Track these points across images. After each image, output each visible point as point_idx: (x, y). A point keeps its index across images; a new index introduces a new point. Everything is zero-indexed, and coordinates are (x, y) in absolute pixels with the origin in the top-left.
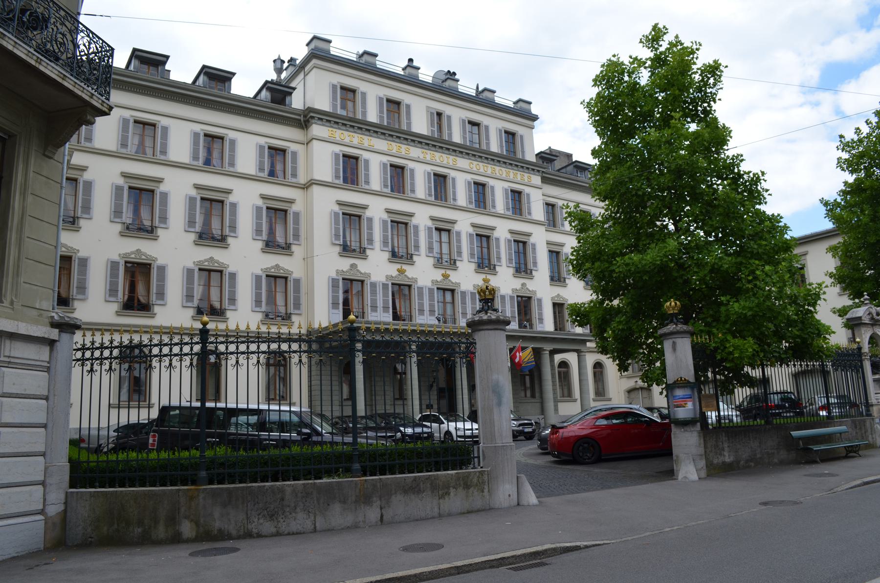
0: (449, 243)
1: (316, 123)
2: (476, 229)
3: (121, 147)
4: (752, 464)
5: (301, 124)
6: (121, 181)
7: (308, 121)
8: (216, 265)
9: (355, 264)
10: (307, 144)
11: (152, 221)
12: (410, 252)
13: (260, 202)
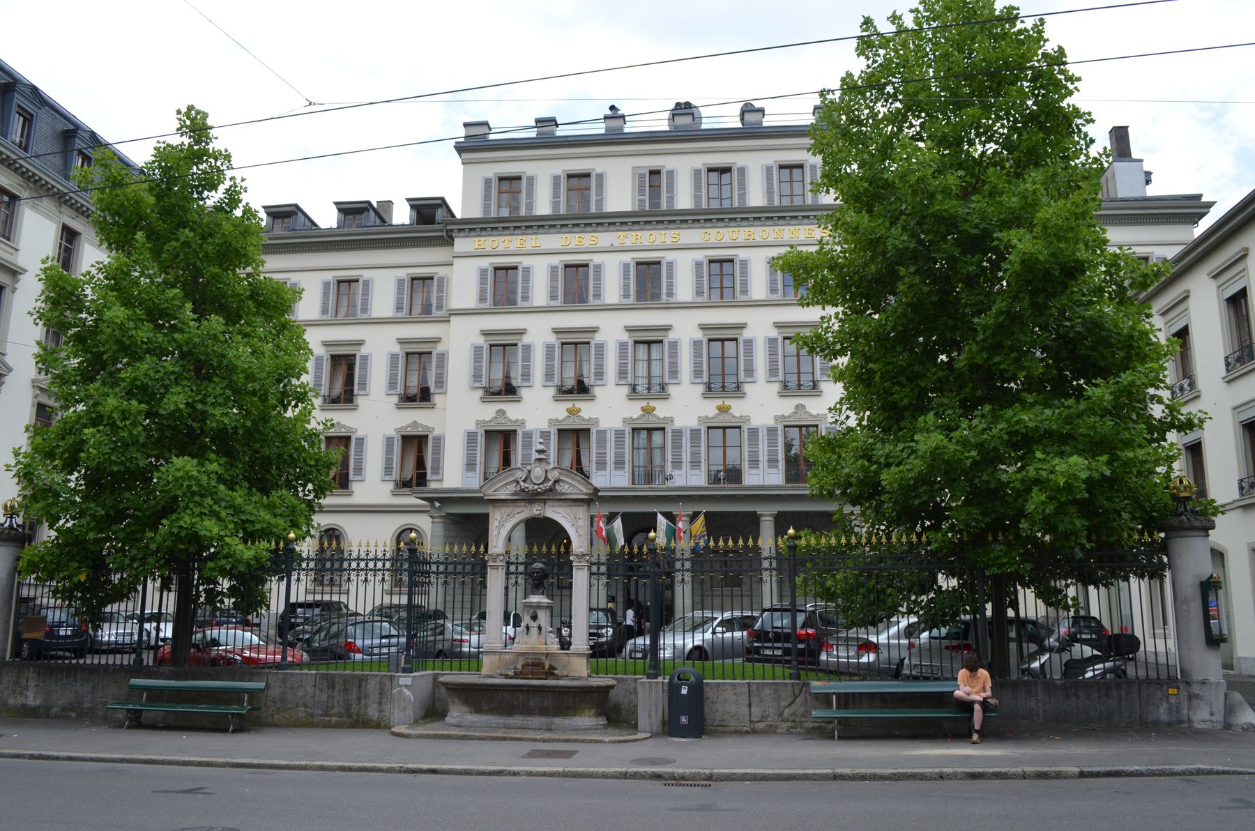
1: (458, 237)
2: (406, 346)
4: (74, 715)
5: (445, 240)
13: (397, 349)
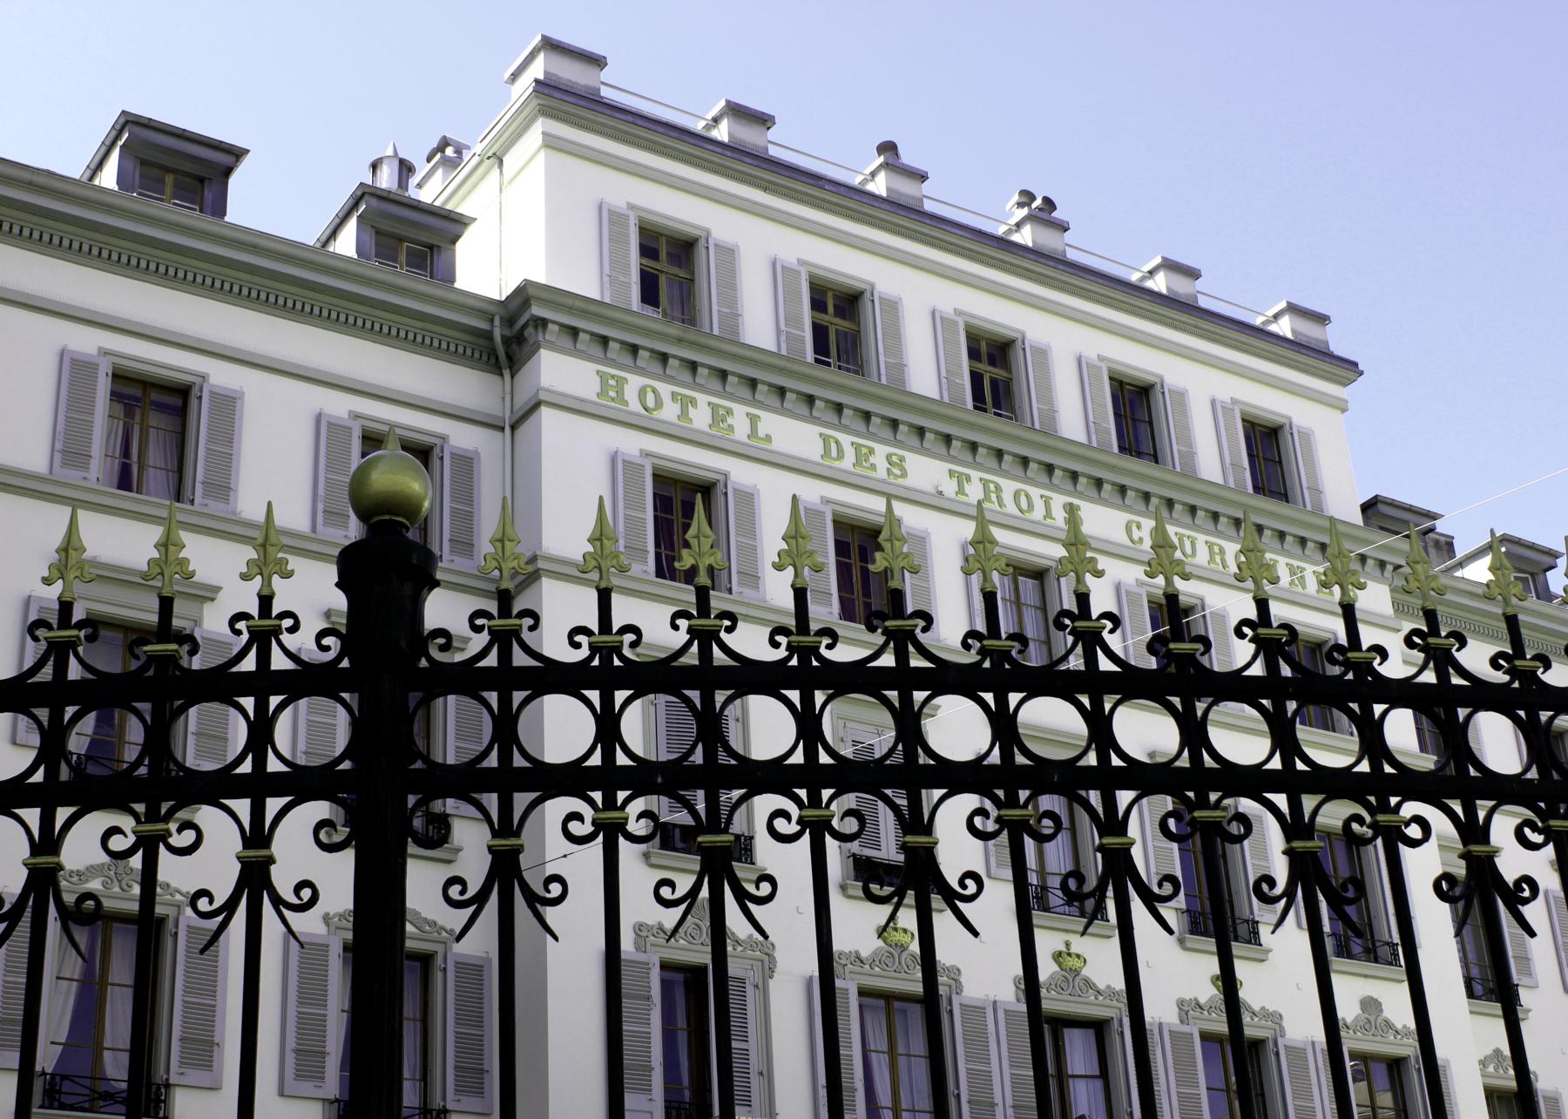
1: (553, 347)
3: (64, 464)
7: (520, 339)
10: (513, 428)
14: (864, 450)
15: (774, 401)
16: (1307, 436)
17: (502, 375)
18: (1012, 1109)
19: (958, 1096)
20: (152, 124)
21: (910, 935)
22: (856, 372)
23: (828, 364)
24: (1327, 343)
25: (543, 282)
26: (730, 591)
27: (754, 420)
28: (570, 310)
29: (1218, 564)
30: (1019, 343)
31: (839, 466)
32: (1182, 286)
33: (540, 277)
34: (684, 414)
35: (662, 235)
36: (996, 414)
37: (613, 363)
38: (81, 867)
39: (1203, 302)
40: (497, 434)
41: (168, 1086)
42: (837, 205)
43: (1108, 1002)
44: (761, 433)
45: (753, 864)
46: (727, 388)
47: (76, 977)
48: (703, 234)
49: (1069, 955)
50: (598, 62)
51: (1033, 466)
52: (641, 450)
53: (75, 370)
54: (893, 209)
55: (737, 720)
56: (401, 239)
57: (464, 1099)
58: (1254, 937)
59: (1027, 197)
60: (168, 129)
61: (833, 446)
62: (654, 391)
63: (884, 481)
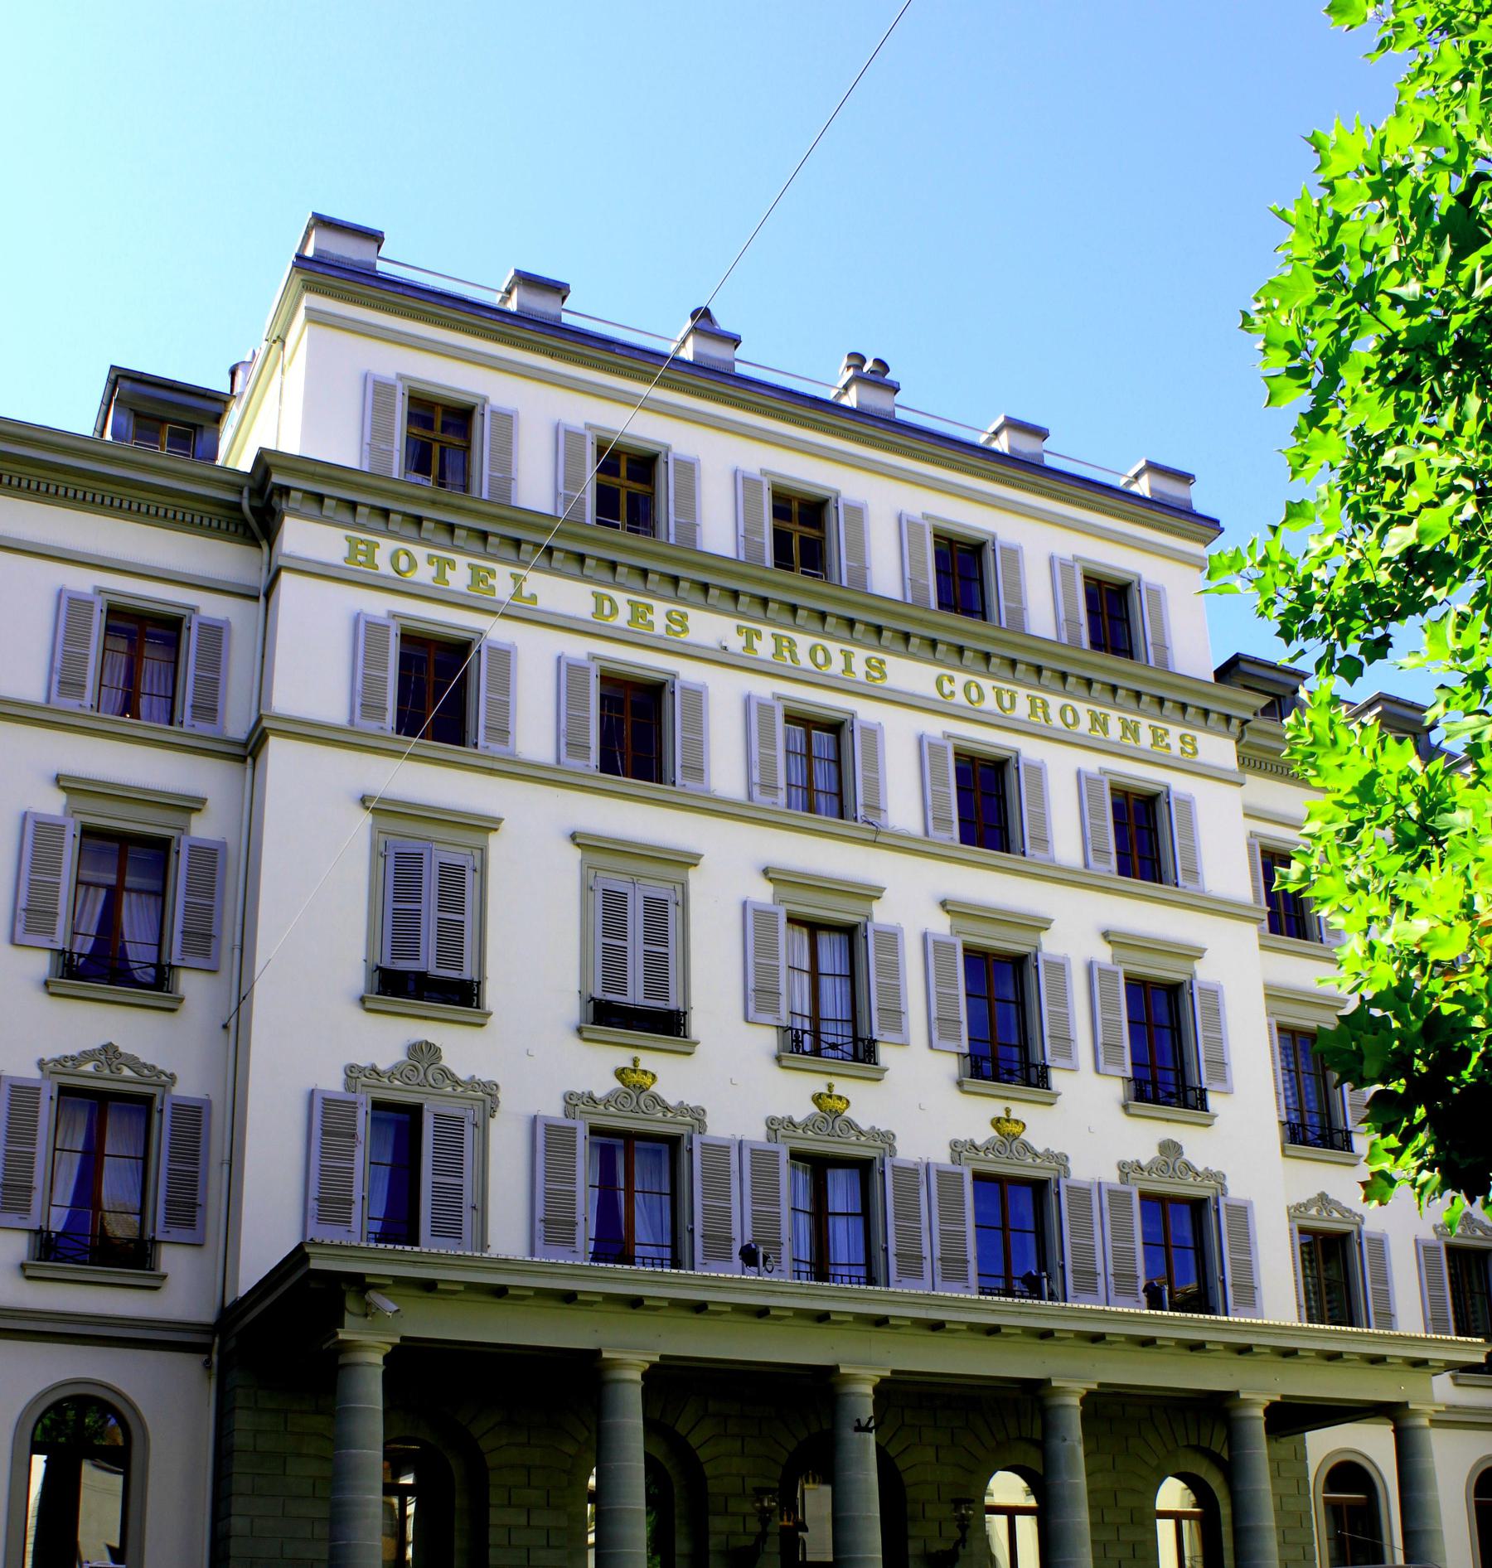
0: (852, 976)
1: (298, 514)
3: (61, 693)
6: (53, 804)
8: (127, 1072)
9: (430, 1045)
11: (160, 945)
12: (864, 1033)
14: (1160, 731)
15: (698, 597)
16: (1156, 594)
17: (260, 547)
18: (940, 1262)
19: (692, 1231)
20: (144, 378)
21: (650, 1076)
22: (646, 533)
23: (617, 526)
24: (1191, 501)
25: (297, 453)
26: (1024, 853)
27: (516, 578)
28: (312, 476)
29: (1039, 718)
30: (1135, 585)
31: (826, 672)
32: (1027, 445)
33: (291, 444)
34: (440, 576)
35: (437, 404)
36: (803, 572)
37: (362, 528)
38: (75, 1053)
39: (1050, 461)
40: (251, 604)
41: (155, 1242)
42: (631, 368)
43: (872, 1143)
44: (525, 593)
45: (1049, 1089)
46: (488, 549)
47: (80, 1149)
48: (990, 538)
49: (1008, 1120)
50: (376, 237)
51: (1168, 705)
52: (773, 694)
53: (71, 607)
54: (691, 371)
55: (677, 904)
56: (163, 421)
57: (174, 1230)
58: (1201, 1103)
59: (857, 359)
60: (162, 381)
61: (607, 604)
62: (824, 650)
63: (1177, 758)
